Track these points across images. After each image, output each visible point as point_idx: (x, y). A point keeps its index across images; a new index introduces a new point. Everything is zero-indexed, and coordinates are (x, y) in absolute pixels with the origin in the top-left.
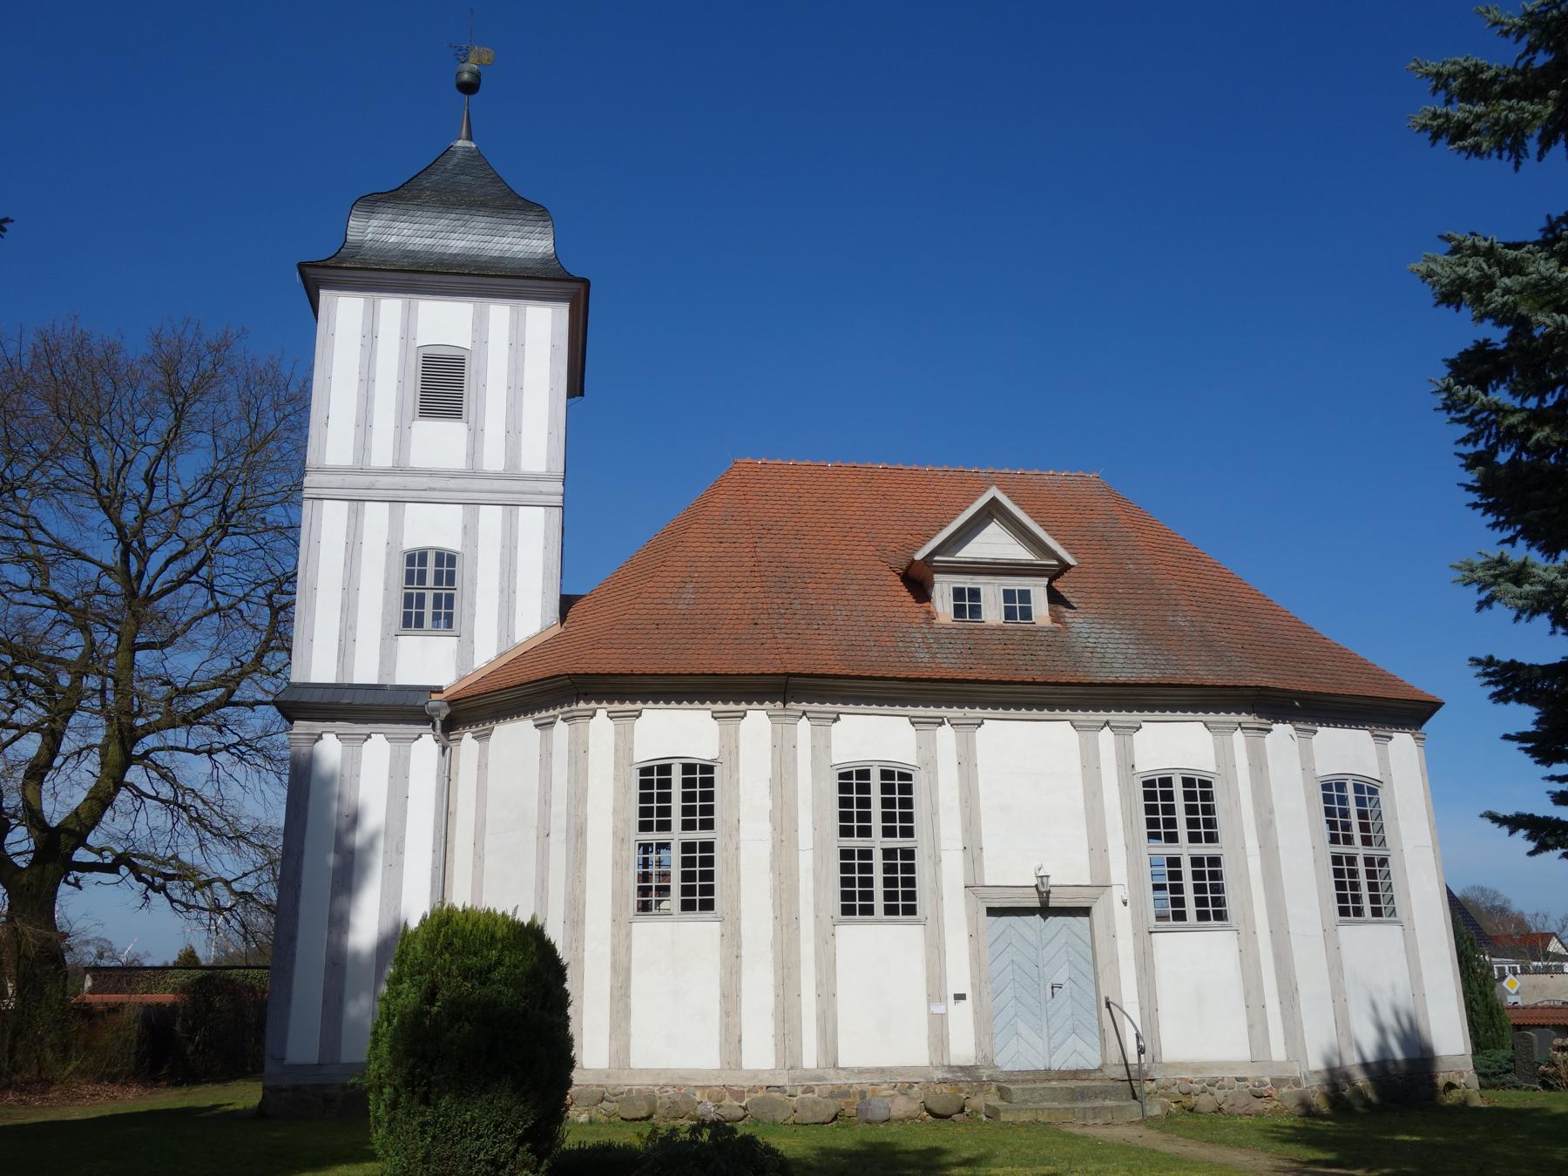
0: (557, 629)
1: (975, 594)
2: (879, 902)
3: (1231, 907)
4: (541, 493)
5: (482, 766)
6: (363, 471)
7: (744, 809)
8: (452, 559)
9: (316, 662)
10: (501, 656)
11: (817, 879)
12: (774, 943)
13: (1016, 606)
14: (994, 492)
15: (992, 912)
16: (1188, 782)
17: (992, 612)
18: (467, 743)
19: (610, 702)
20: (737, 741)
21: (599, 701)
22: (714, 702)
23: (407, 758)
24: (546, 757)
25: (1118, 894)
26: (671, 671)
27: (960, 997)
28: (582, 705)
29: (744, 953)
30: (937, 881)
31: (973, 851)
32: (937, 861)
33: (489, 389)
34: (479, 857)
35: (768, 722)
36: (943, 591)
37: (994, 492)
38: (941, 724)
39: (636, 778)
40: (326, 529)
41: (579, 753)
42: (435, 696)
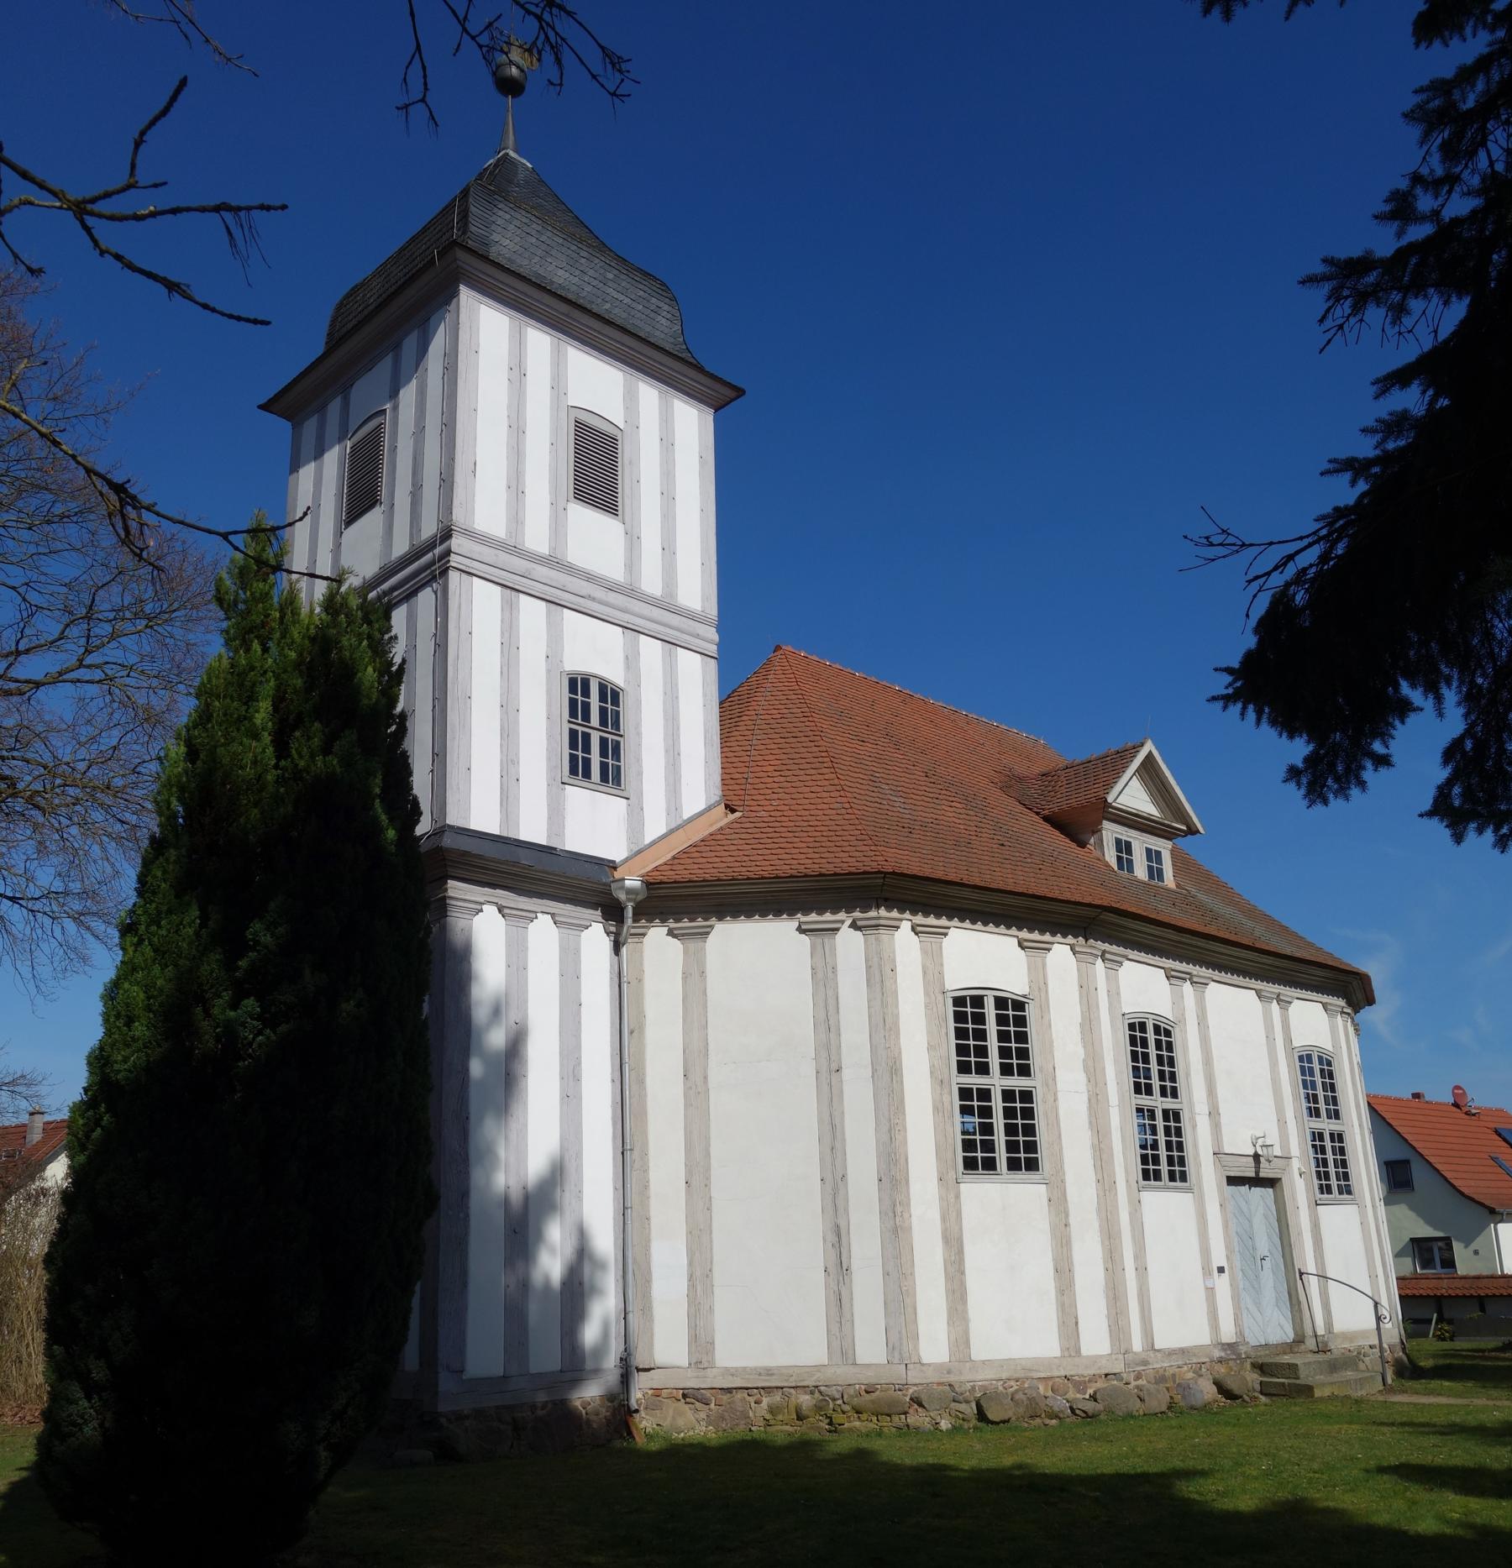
2: (1001, 1155)
3: (1044, 1154)
4: (697, 636)
12: (1099, 1211)
16: (1001, 1003)
19: (914, 913)
21: (902, 911)
22: (1020, 929)
25: (1296, 1164)
28: (883, 912)
29: (1072, 1220)
32: (1194, 1127)
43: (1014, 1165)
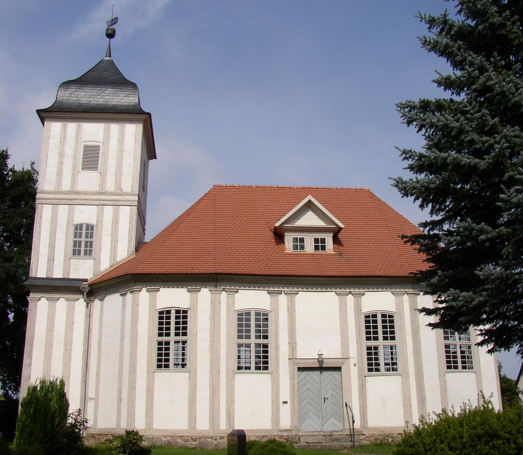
0: (134, 256)
1: (302, 240)
4: (129, 200)
5: (102, 311)
6: (101, 193)
7: (199, 327)
8: (92, 227)
9: (40, 268)
10: (111, 266)
11: (228, 356)
13: (320, 245)
14: (309, 197)
15: (300, 369)
17: (309, 247)
18: (97, 303)
20: (197, 301)
23: (74, 307)
24: (124, 306)
25: (352, 361)
26: (281, 274)
27: (285, 402)
30: (277, 355)
31: (293, 345)
33: (109, 160)
34: (100, 347)
35: (209, 293)
36: (289, 238)
37: (309, 197)
38: (281, 293)
39: (157, 315)
40: (44, 216)
41: (135, 305)
42: (84, 283)
43: (464, 368)
